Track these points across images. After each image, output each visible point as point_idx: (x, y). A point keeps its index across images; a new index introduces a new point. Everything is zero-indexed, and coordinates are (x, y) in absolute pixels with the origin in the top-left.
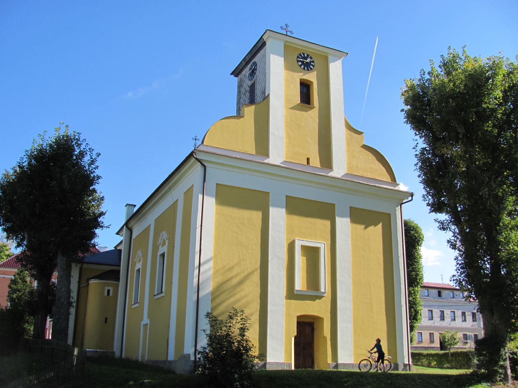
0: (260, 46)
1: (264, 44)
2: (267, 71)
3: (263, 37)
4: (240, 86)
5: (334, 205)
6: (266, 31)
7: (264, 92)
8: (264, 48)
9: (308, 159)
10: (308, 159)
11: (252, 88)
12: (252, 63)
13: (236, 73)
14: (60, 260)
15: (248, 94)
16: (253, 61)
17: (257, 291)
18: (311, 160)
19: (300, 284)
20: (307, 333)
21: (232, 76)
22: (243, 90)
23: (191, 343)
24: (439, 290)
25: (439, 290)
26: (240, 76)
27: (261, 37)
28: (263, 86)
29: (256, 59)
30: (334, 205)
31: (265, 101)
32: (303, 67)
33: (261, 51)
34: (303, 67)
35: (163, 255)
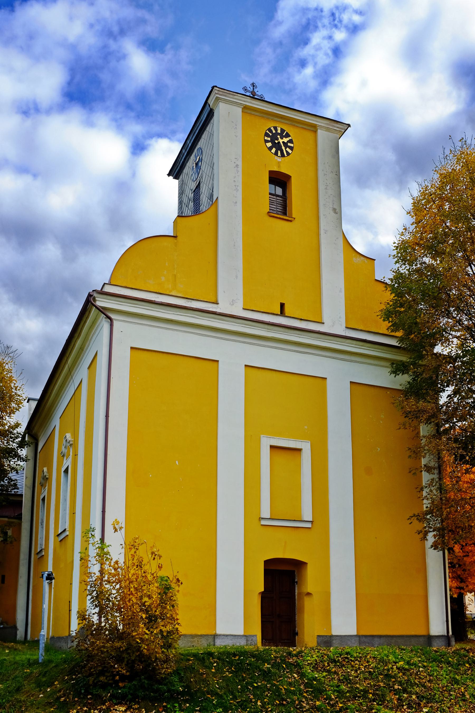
1: (211, 114)
2: (215, 161)
4: (181, 193)
5: (269, 171)
6: (213, 87)
8: (212, 121)
9: (282, 305)
10: (282, 305)
14: (49, 642)
15: (191, 204)
16: (198, 147)
17: (173, 294)
20: (282, 587)
21: (171, 177)
22: (185, 200)
26: (181, 177)
27: (206, 102)
28: (210, 187)
29: (201, 144)
30: (269, 171)
32: (274, 150)
34: (274, 150)
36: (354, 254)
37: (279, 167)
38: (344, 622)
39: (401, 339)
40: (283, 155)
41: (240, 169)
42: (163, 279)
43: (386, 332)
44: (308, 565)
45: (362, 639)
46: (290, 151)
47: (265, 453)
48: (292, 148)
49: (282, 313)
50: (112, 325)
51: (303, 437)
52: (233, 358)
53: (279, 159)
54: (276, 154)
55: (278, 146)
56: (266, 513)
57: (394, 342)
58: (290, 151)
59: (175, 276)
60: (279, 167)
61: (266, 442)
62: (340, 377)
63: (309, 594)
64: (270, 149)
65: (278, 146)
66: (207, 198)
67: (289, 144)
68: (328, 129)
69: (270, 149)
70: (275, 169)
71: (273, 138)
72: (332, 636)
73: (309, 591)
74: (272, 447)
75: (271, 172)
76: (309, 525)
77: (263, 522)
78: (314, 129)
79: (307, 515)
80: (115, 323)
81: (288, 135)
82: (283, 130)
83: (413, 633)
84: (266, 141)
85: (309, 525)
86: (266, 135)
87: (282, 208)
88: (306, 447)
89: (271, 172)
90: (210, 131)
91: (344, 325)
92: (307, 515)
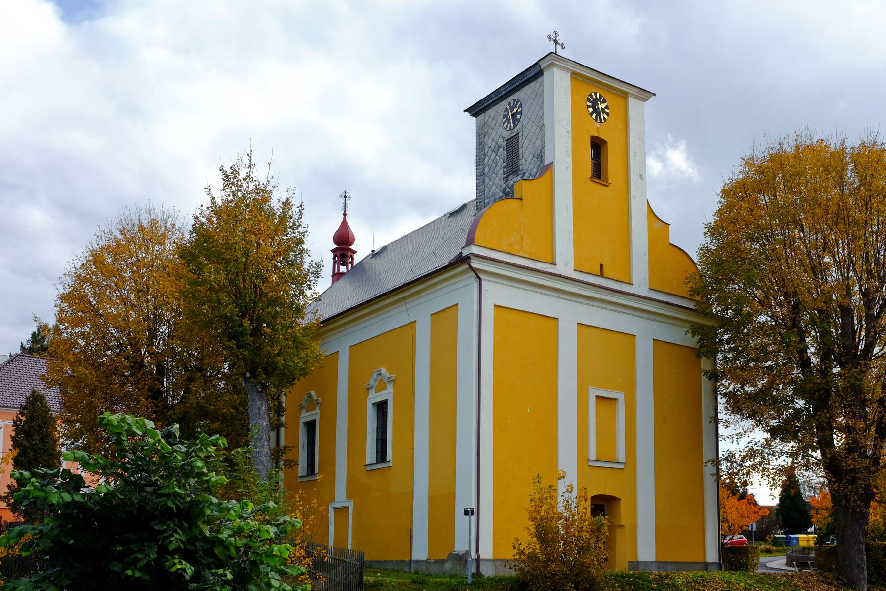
0: (532, 75)
1: (540, 73)
2: (547, 121)
3: (541, 63)
7: (540, 156)
11: (513, 145)
12: (510, 99)
13: (476, 110)
15: (503, 153)
16: (516, 96)
18: (605, 268)
19: (370, 456)
21: (467, 114)
23: (490, 539)
24: (475, 512)
25: (475, 512)
26: (482, 117)
27: (538, 62)
28: (537, 145)
29: (519, 95)
31: (547, 175)
33: (532, 84)
35: (381, 407)
36: (654, 218)
37: (598, 132)
38: (646, 551)
39: (697, 303)
40: (601, 121)
41: (570, 135)
42: (513, 240)
43: (687, 296)
44: (622, 502)
45: (659, 564)
46: (606, 117)
47: (592, 401)
48: (608, 114)
49: (602, 275)
50: (480, 285)
51: (618, 388)
52: (569, 315)
53: (598, 125)
54: (596, 119)
55: (596, 111)
56: (593, 456)
57: (691, 305)
58: (606, 117)
59: (522, 237)
60: (598, 132)
61: (593, 392)
62: (645, 333)
63: (621, 526)
64: (591, 114)
65: (596, 111)
66: (531, 156)
67: (606, 110)
68: (637, 97)
69: (591, 114)
70: (596, 135)
71: (595, 103)
72: (638, 562)
73: (622, 523)
74: (597, 397)
75: (592, 137)
76: (622, 466)
77: (591, 464)
78: (625, 95)
79: (622, 457)
80: (483, 282)
81: (605, 101)
82: (601, 96)
83: (694, 561)
84: (588, 107)
85: (622, 466)
86: (588, 100)
87: (598, 172)
88: (620, 396)
89: (592, 137)
90: (536, 89)
91: (648, 287)
92: (622, 457)
